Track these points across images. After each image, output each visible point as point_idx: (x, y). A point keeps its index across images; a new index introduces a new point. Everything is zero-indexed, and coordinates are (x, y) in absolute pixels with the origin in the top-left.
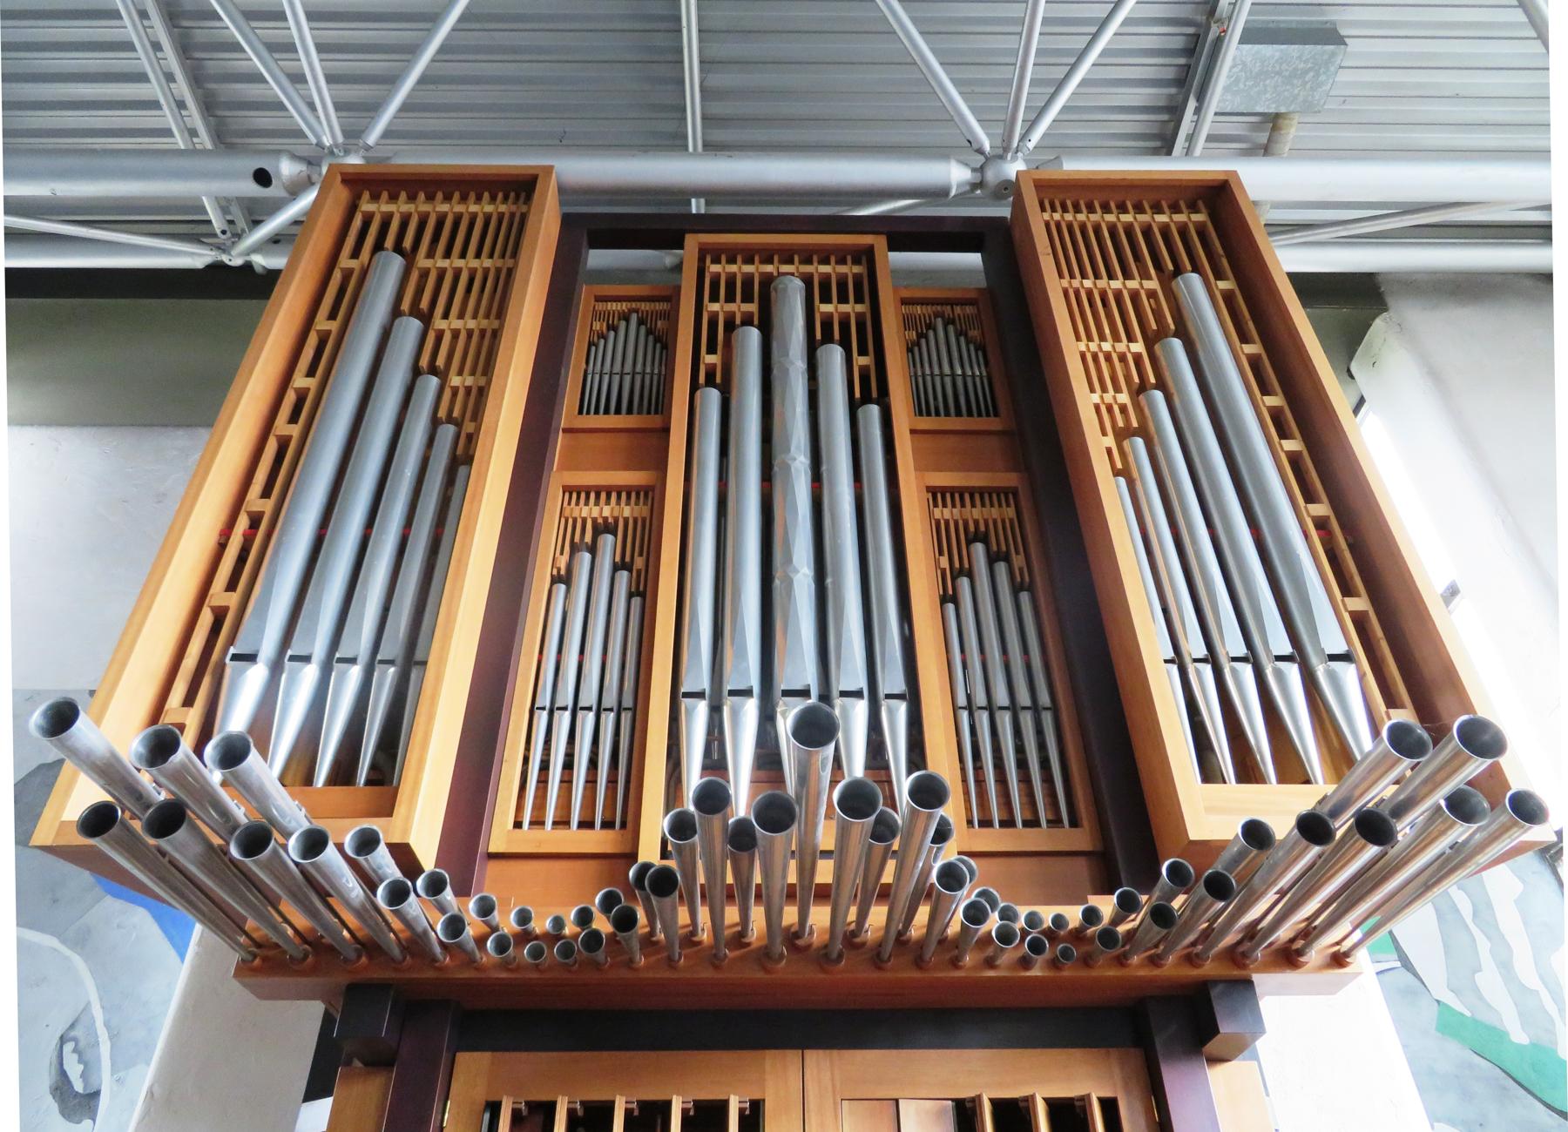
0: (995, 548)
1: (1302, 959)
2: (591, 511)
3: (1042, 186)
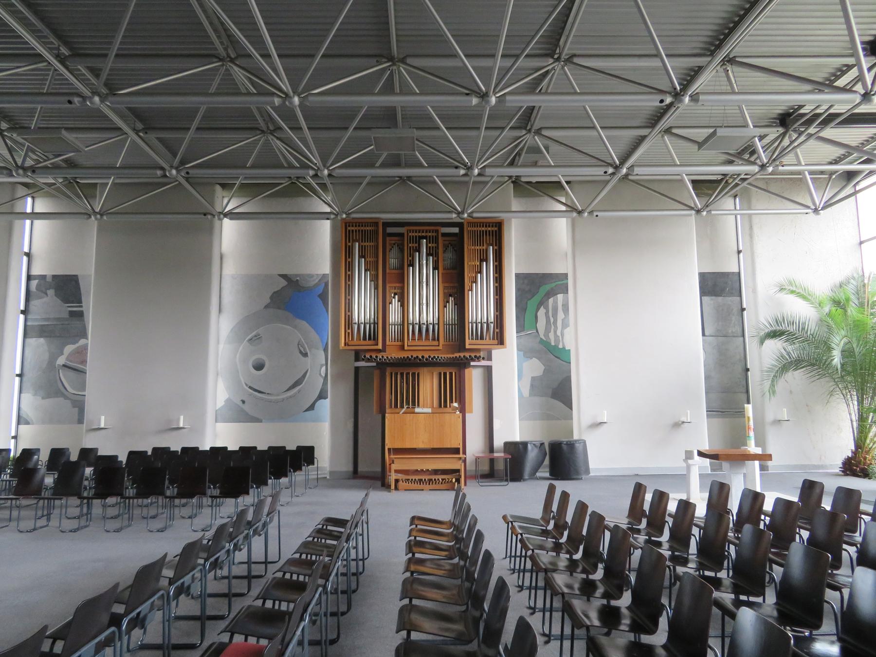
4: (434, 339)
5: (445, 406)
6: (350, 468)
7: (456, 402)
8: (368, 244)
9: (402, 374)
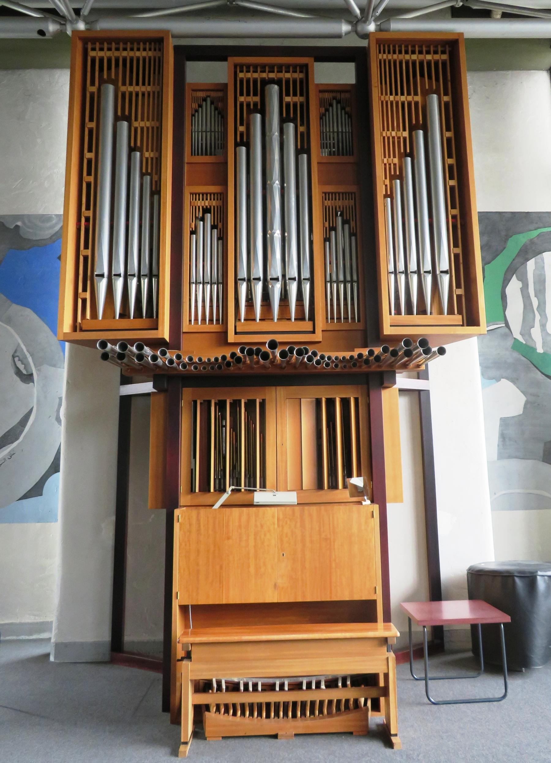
0: (345, 218)
1: (408, 367)
2: (201, 203)
3: (379, 42)
4: (300, 317)
5: (334, 486)
6: (106, 636)
7: (359, 475)
8: (137, 89)
9: (221, 405)
